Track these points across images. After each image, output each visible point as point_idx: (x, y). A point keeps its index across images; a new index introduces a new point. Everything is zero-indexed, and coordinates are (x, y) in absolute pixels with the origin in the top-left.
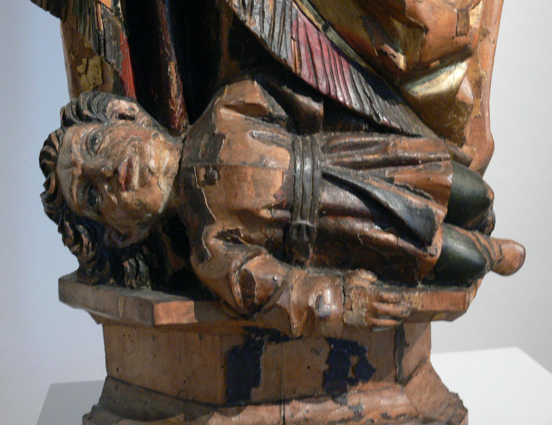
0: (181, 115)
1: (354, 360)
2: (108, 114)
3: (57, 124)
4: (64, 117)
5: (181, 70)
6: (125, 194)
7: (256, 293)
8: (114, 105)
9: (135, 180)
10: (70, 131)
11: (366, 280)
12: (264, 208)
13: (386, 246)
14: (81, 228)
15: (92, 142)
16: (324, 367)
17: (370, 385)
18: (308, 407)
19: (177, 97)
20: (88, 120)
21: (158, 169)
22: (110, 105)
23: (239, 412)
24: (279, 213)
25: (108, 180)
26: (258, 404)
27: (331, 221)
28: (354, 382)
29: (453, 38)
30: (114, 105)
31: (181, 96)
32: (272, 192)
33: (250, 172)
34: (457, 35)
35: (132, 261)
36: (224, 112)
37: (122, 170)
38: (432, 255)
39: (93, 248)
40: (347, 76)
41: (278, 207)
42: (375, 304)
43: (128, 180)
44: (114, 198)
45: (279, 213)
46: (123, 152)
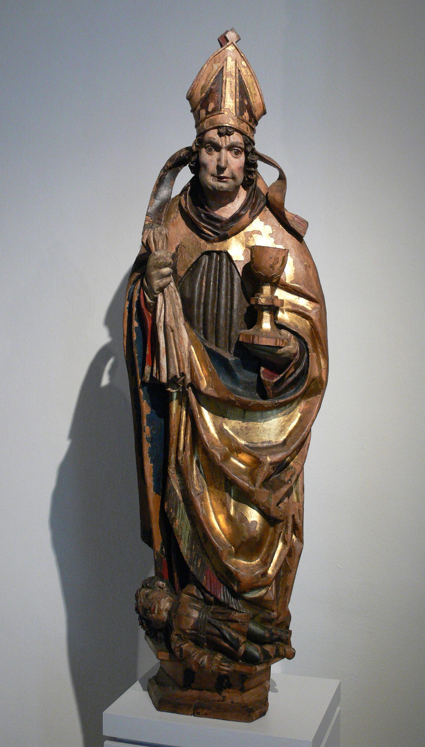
0: (179, 589)
1: (226, 680)
2: (156, 585)
3: (141, 586)
4: (142, 585)
5: (178, 575)
6: (153, 615)
7: (183, 655)
8: (158, 583)
9: (156, 612)
10: (143, 589)
11: (219, 657)
12: (188, 629)
13: (226, 648)
14: (143, 621)
15: (147, 595)
16: (216, 681)
17: (231, 690)
18: (209, 693)
19: (177, 583)
20: (148, 588)
21: (163, 609)
22: (156, 583)
23: (187, 690)
24: (193, 632)
25: (149, 610)
26: (193, 689)
27: (210, 636)
28: (225, 688)
29: (252, 584)
30: (158, 583)
31: (178, 583)
32: (190, 625)
33: (184, 617)
34: (254, 583)
35: (160, 633)
36: (184, 594)
37: (152, 608)
38: (240, 654)
39: (147, 628)
40: (222, 590)
41: (192, 630)
42: (220, 666)
43: (154, 610)
44: (150, 615)
45: (193, 632)
46: (154, 602)
